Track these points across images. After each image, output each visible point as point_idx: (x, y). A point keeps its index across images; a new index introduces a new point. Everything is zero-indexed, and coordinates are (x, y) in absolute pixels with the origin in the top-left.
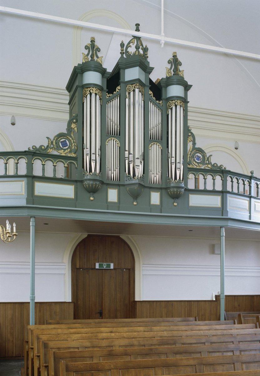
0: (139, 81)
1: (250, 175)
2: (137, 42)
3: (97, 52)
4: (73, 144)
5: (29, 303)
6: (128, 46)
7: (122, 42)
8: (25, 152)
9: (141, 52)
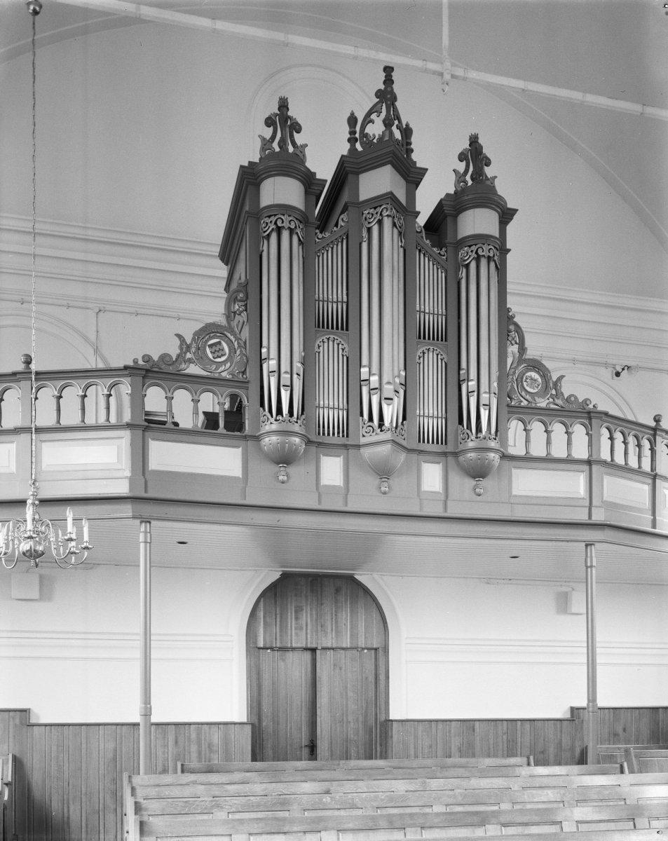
0: (391, 197)
1: (653, 424)
2: (388, 111)
3: (295, 133)
4: (238, 352)
5: (136, 725)
6: (367, 120)
7: (352, 114)
8: (126, 368)
9: (398, 135)
